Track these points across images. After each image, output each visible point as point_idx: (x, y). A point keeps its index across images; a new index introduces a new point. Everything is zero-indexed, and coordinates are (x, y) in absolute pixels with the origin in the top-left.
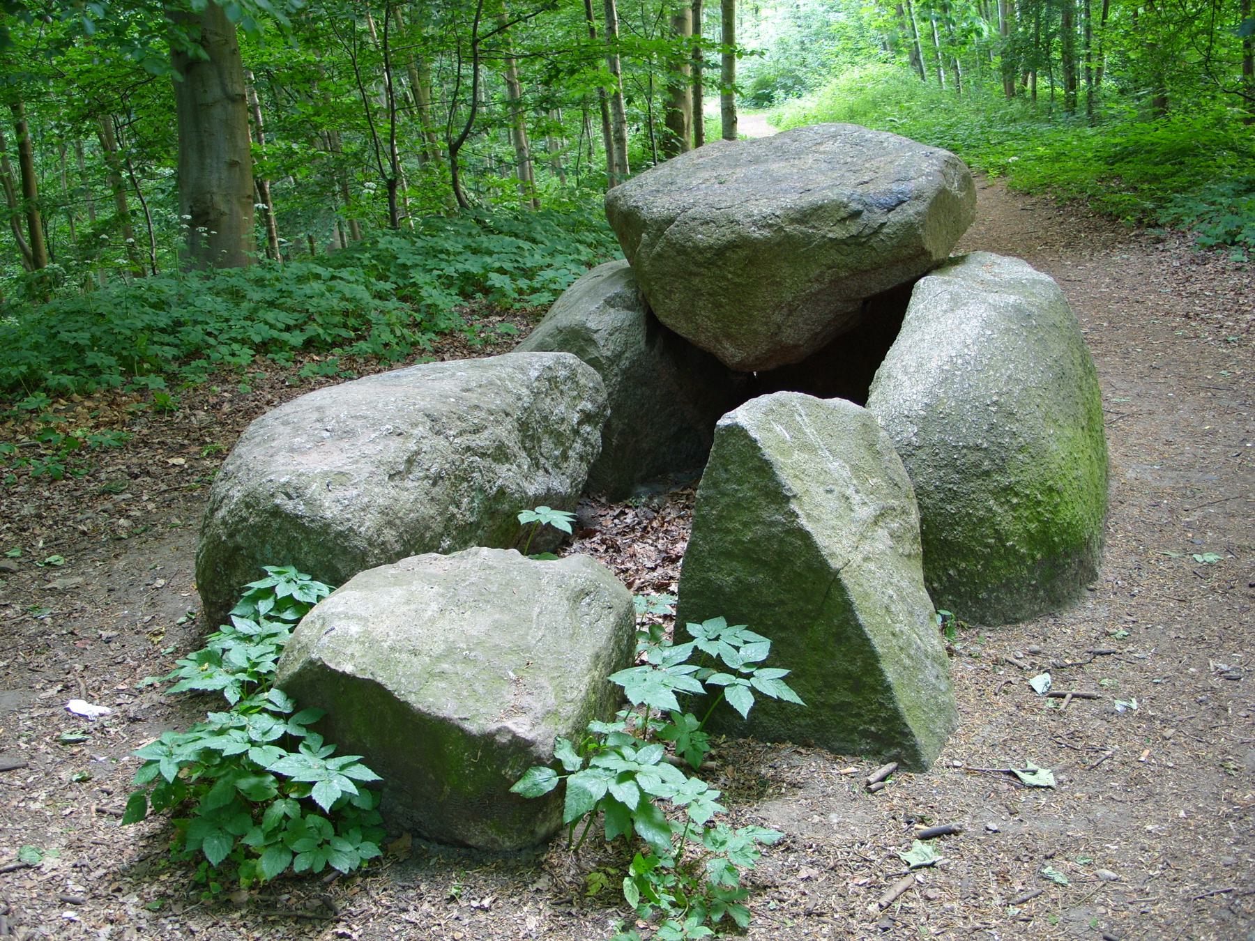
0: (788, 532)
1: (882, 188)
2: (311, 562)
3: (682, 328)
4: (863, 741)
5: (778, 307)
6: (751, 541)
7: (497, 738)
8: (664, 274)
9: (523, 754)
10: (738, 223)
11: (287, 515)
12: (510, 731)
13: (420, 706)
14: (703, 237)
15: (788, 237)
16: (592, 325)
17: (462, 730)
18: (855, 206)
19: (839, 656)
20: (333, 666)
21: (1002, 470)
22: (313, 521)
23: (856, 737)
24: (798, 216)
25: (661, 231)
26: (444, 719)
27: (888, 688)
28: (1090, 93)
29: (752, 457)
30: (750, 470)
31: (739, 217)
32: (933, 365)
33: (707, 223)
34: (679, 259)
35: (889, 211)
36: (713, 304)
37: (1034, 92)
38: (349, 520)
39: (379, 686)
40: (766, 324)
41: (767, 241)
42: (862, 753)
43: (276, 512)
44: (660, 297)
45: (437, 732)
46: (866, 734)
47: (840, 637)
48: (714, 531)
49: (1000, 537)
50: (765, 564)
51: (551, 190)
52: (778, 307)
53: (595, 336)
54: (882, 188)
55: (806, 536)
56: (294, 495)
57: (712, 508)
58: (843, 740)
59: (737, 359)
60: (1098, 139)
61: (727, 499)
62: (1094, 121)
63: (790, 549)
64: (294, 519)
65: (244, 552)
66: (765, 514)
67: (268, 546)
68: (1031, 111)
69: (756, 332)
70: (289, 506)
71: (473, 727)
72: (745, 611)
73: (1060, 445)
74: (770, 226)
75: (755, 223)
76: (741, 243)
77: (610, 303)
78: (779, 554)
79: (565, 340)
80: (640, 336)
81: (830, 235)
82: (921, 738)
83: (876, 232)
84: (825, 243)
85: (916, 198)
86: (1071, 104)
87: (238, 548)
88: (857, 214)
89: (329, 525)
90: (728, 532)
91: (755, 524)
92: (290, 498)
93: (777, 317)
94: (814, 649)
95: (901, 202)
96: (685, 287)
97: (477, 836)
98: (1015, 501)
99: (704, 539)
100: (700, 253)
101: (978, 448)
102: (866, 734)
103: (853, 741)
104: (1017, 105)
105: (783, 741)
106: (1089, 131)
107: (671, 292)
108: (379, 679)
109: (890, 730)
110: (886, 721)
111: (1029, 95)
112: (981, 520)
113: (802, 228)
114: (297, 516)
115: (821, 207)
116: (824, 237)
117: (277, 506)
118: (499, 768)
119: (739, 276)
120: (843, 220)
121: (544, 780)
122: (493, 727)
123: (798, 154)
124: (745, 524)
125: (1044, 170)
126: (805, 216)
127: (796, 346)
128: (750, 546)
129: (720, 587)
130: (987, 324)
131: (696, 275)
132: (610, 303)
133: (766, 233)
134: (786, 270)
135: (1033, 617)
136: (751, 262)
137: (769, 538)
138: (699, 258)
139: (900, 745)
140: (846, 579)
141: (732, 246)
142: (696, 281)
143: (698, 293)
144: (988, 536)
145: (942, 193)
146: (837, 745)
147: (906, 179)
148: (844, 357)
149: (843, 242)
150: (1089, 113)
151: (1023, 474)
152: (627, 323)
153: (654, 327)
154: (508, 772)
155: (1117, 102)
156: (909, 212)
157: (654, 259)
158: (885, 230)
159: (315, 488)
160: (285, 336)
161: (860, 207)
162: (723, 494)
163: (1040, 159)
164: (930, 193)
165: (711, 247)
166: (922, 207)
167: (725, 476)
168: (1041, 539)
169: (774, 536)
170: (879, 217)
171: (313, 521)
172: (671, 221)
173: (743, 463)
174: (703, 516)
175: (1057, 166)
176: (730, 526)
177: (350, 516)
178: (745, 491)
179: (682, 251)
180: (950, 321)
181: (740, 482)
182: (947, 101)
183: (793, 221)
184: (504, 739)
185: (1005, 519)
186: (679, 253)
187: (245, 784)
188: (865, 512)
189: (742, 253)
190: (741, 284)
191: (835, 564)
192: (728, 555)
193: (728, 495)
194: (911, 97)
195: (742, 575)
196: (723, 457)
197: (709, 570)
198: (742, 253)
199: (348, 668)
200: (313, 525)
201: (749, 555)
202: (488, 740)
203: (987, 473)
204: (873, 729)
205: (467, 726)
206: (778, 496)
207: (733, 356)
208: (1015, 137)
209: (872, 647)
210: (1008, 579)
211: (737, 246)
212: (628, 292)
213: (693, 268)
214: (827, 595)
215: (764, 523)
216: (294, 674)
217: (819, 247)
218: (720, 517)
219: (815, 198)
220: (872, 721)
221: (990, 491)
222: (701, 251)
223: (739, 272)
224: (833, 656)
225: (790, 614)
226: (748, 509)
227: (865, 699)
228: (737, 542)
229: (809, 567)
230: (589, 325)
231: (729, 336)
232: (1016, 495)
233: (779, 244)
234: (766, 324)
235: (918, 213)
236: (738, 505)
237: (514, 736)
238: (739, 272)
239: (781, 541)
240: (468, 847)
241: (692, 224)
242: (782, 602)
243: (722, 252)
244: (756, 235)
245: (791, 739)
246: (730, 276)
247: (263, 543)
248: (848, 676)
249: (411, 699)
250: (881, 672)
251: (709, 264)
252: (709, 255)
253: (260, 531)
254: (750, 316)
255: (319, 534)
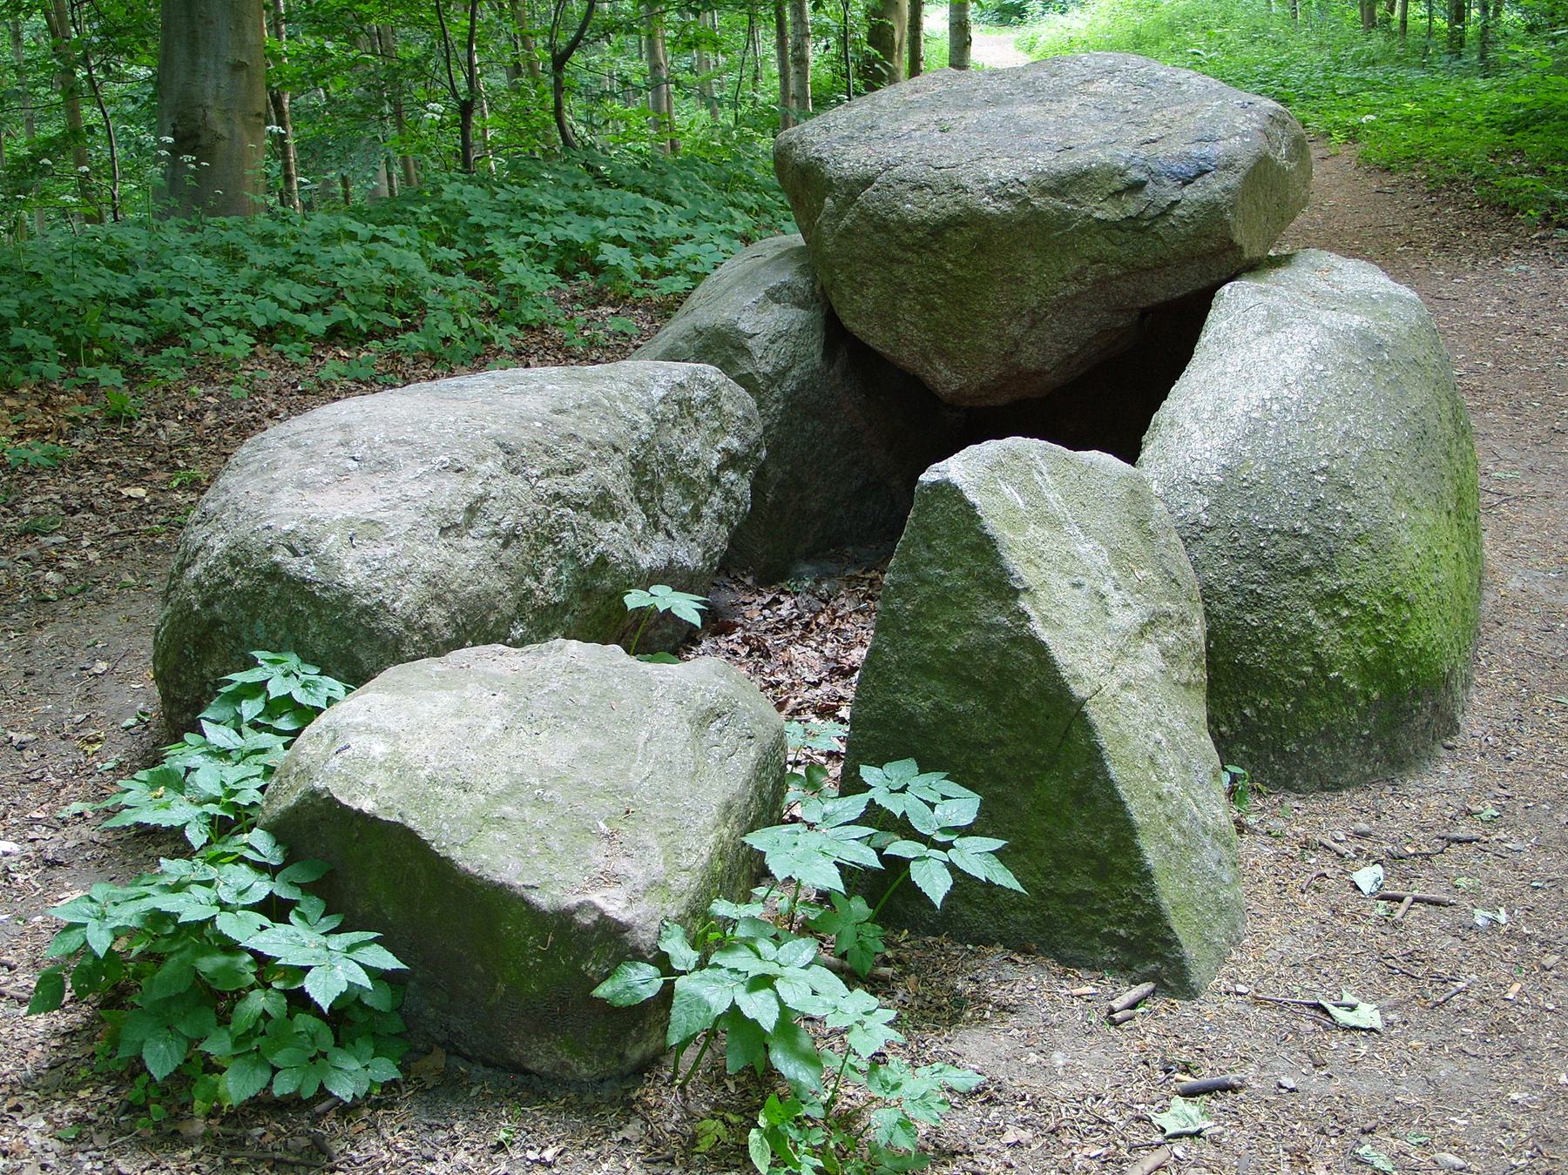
0: (1014, 641)
1: (1176, 150)
2: (320, 648)
3: (876, 337)
4: (1107, 950)
5: (1016, 314)
6: (959, 651)
7: (578, 917)
8: (854, 259)
9: (614, 942)
10: (965, 189)
11: (289, 577)
12: (596, 908)
13: (468, 865)
14: (912, 207)
15: (1038, 214)
16: (745, 326)
17: (527, 903)
18: (1135, 174)
19: (1078, 823)
20: (345, 801)
21: (1328, 568)
22: (327, 589)
23: (1097, 942)
24: (1053, 184)
25: (852, 196)
26: (502, 885)
27: (1147, 875)
28: (1485, 29)
29: (968, 530)
30: (964, 548)
31: (967, 181)
32: (1237, 409)
33: (921, 188)
34: (876, 237)
35: (1185, 184)
36: (923, 305)
37: (1404, 23)
38: (379, 590)
39: (411, 834)
40: (999, 338)
41: (1005, 218)
42: (1104, 966)
43: (274, 573)
44: (847, 291)
45: (489, 905)
46: (1111, 939)
47: (1081, 797)
48: (907, 634)
49: (1321, 665)
50: (978, 685)
51: (696, 129)
52: (1016, 314)
53: (750, 343)
54: (1176, 151)
55: (1040, 648)
56: (302, 550)
57: (906, 601)
58: (1077, 946)
59: (953, 387)
60: (1493, 95)
61: (928, 589)
62: (1488, 68)
63: (1015, 665)
64: (299, 585)
65: (225, 629)
66: (982, 614)
67: (260, 622)
68: (1398, 51)
69: (982, 350)
70: (293, 565)
71: (542, 900)
72: (946, 752)
73: (1415, 535)
74: (1012, 196)
75: (989, 191)
76: (968, 220)
77: (774, 296)
78: (999, 672)
79: (705, 346)
80: (816, 349)
81: (1098, 215)
82: (1191, 949)
83: (1164, 214)
84: (1090, 226)
85: (1225, 168)
86: (1456, 42)
87: (216, 623)
88: (1138, 186)
89: (350, 596)
90: (927, 636)
91: (967, 627)
92: (296, 554)
93: (1015, 330)
94: (1043, 813)
95: (1202, 172)
96: (883, 279)
97: (541, 1056)
98: (1345, 613)
99: (892, 644)
100: (908, 230)
101: (1295, 534)
102: (1111, 939)
103: (1092, 949)
104: (1378, 40)
105: (991, 944)
106: (1481, 84)
107: (862, 284)
108: (411, 824)
109: (1147, 935)
110: (1141, 922)
111: (1396, 26)
112: (1295, 638)
113: (1058, 202)
114: (304, 580)
115: (1086, 173)
116: (1088, 216)
117: (276, 565)
118: (578, 961)
119: (962, 267)
120: (1118, 193)
121: (641, 981)
122: (572, 901)
123: (1058, 95)
124: (952, 627)
125: (1412, 136)
126: (1064, 184)
127: (1039, 373)
128: (958, 658)
129: (912, 716)
130: (1318, 354)
131: (900, 261)
132: (774, 296)
133: (1005, 206)
134: (1031, 263)
135: (1362, 782)
136: (981, 247)
137: (987, 648)
138: (906, 237)
139: (1160, 957)
140: (1094, 713)
141: (954, 223)
142: (900, 271)
143: (902, 288)
144: (1302, 663)
145: (1263, 161)
146: (1069, 952)
147: (1212, 139)
148: (1109, 391)
149: (1116, 225)
150: (1482, 57)
151: (1358, 575)
152: (797, 326)
153: (835, 335)
154: (590, 967)
155: (1524, 44)
156: (1214, 187)
157: (841, 236)
158: (1177, 212)
159: (331, 543)
160: (301, 319)
161: (1143, 176)
162: (924, 582)
163: (1407, 120)
164: (1245, 161)
165: (924, 223)
166: (1233, 180)
167: (927, 555)
168: (1380, 671)
169: (993, 646)
170: (1170, 192)
171: (327, 589)
172: (867, 182)
173: (954, 538)
174: (892, 612)
175: (1432, 131)
176: (931, 627)
177: (380, 585)
178: (955, 579)
179: (882, 226)
180: (1265, 347)
181: (948, 564)
182: (1277, 29)
183: (1044, 191)
184: (587, 920)
185: (1330, 641)
186: (877, 228)
187: (209, 964)
188: (1127, 619)
189: (969, 234)
190: (964, 279)
191: (1079, 690)
192: (926, 670)
193: (930, 583)
194: (1225, 21)
195: (944, 700)
196: (926, 528)
197: (897, 690)
198: (969, 234)
199: (367, 805)
200: (326, 595)
201: (958, 671)
202: (564, 917)
203: (1307, 571)
204: (1122, 932)
205: (534, 897)
206: (1003, 588)
207: (949, 382)
208: (1372, 87)
209: (1126, 813)
210: (1329, 726)
211: (963, 224)
212: (801, 282)
213: (898, 253)
214: (1066, 735)
215: (979, 626)
216: (288, 809)
217: (1081, 230)
218: (917, 615)
219: (1079, 160)
220: (1121, 921)
221: (1309, 598)
222: (909, 228)
223: (963, 261)
224: (1070, 822)
225: (1011, 760)
226: (958, 604)
227: (1113, 888)
228: (939, 652)
229: (1042, 694)
230: (741, 326)
231: (942, 353)
232: (1348, 604)
233: (1022, 224)
234: (999, 338)
235: (1226, 190)
236: (943, 598)
237: (602, 915)
238: (963, 261)
239: (1004, 654)
240: (527, 1072)
241: (898, 188)
242: (999, 742)
243: (939, 231)
244: (990, 209)
245: (1002, 940)
246: (949, 266)
247: (254, 617)
248: (1091, 853)
249: (456, 854)
250: (1139, 850)
251: (920, 247)
252: (920, 234)
253: (250, 601)
254: (976, 325)
255: (335, 609)
